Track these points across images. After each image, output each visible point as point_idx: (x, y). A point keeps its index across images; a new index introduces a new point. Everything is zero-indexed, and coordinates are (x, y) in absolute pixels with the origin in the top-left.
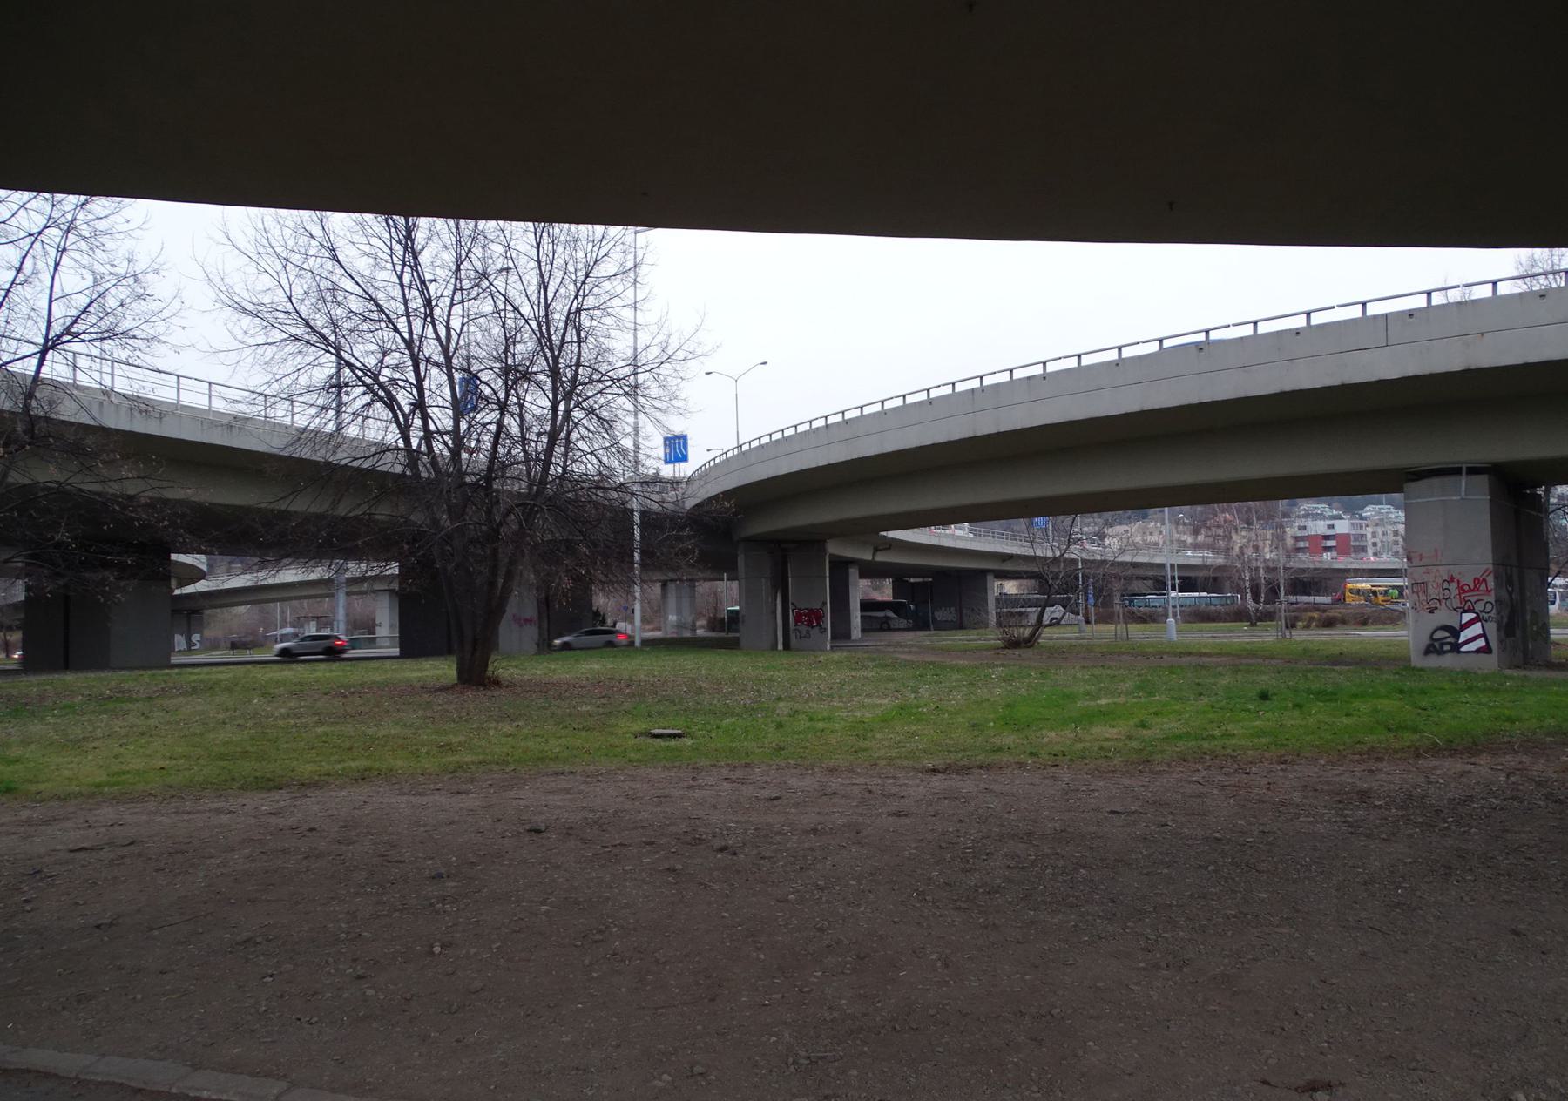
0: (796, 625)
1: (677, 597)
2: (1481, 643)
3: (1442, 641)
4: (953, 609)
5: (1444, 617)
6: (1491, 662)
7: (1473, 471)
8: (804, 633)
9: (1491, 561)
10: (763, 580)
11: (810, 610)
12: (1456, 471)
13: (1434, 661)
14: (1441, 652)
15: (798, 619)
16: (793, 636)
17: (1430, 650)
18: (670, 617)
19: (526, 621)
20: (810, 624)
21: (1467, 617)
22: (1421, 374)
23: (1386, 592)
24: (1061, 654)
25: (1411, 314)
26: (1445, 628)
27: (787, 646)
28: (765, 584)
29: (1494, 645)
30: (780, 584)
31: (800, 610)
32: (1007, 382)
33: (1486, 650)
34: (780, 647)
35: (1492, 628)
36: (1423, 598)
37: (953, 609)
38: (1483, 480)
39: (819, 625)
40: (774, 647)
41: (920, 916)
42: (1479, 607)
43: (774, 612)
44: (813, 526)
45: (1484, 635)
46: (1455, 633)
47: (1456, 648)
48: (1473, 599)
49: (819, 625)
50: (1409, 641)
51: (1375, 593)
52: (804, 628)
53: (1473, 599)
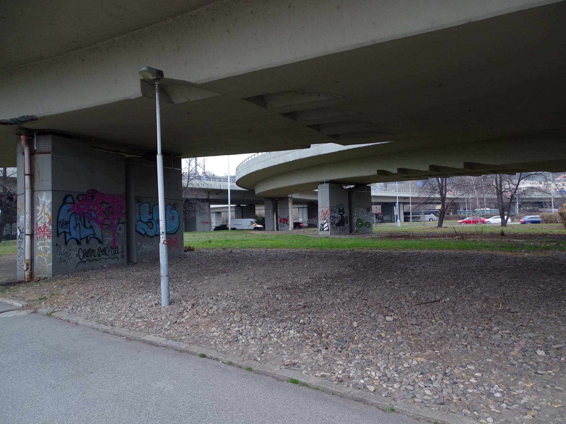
1: (302, 213)
4: (389, 216)
6: (329, 233)
7: (326, 182)
8: (282, 225)
9: (51, 189)
10: (270, 210)
11: (284, 219)
12: (323, 183)
15: (280, 221)
16: (279, 226)
18: (300, 219)
19: (206, 223)
20: (284, 223)
21: (325, 221)
27: (277, 229)
29: (329, 229)
30: (275, 210)
32: (141, 97)
33: (328, 230)
34: (275, 229)
35: (329, 224)
37: (389, 216)
38: (328, 184)
39: (287, 223)
40: (274, 230)
42: (327, 219)
43: (273, 219)
44: (263, 192)
45: (328, 226)
48: (326, 216)
49: (287, 223)
52: (282, 224)
53: (326, 216)
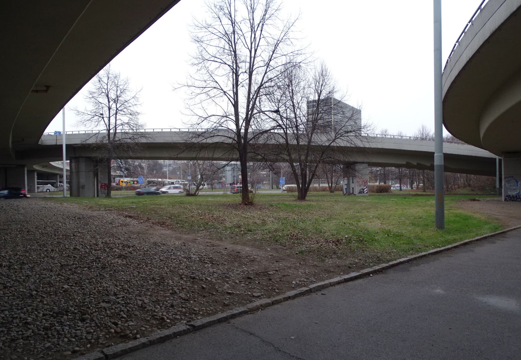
0: (101, 189)
2: (366, 191)
3: (362, 191)
5: (362, 187)
10: (91, 173)
13: (360, 195)
14: (361, 193)
15: (101, 187)
16: (100, 193)
17: (360, 193)
21: (365, 187)
22: (490, 157)
23: (129, 182)
24: (200, 196)
25: (158, 132)
26: (362, 189)
27: (98, 196)
28: (91, 174)
31: (102, 184)
34: (96, 196)
36: (358, 184)
40: (94, 196)
41: (280, 280)
46: (364, 190)
47: (364, 192)
50: (35, 193)
51: (127, 182)
